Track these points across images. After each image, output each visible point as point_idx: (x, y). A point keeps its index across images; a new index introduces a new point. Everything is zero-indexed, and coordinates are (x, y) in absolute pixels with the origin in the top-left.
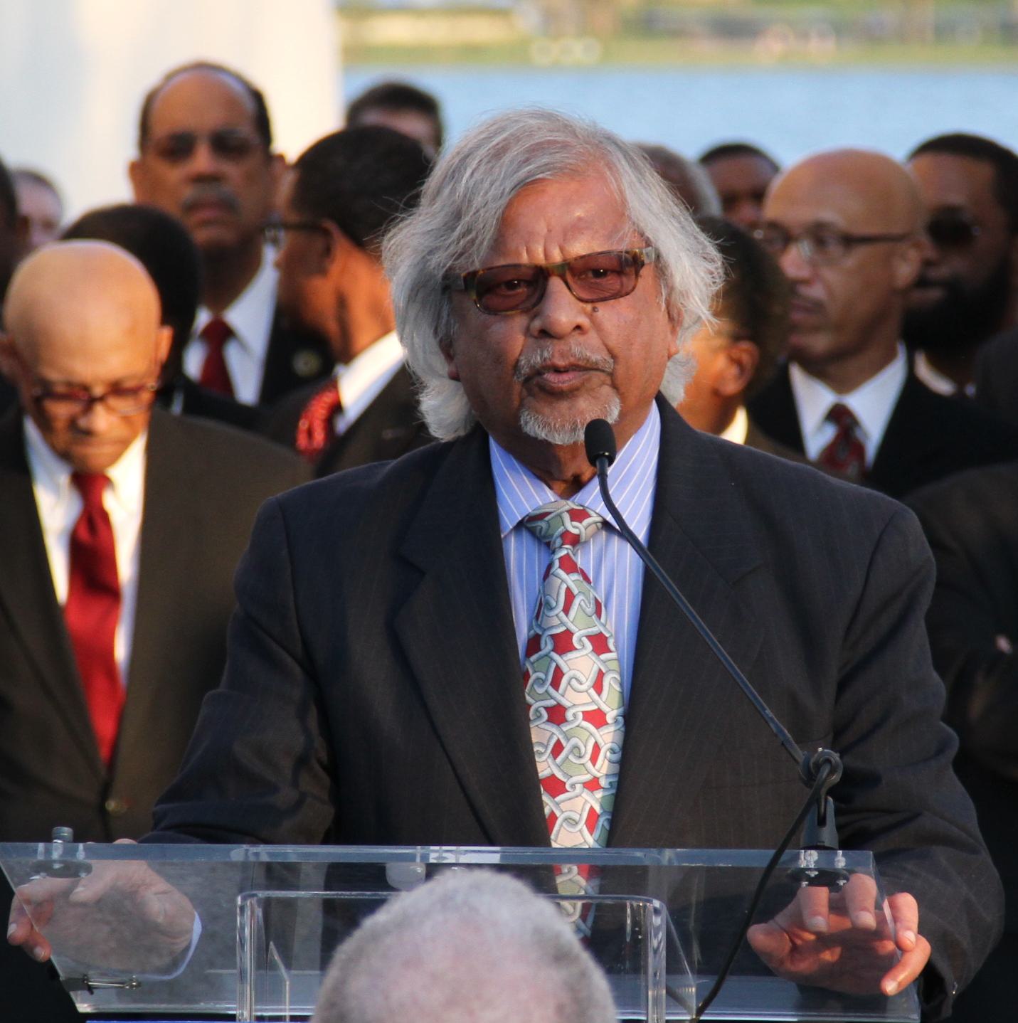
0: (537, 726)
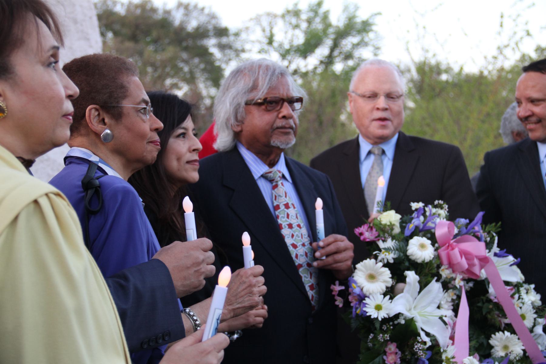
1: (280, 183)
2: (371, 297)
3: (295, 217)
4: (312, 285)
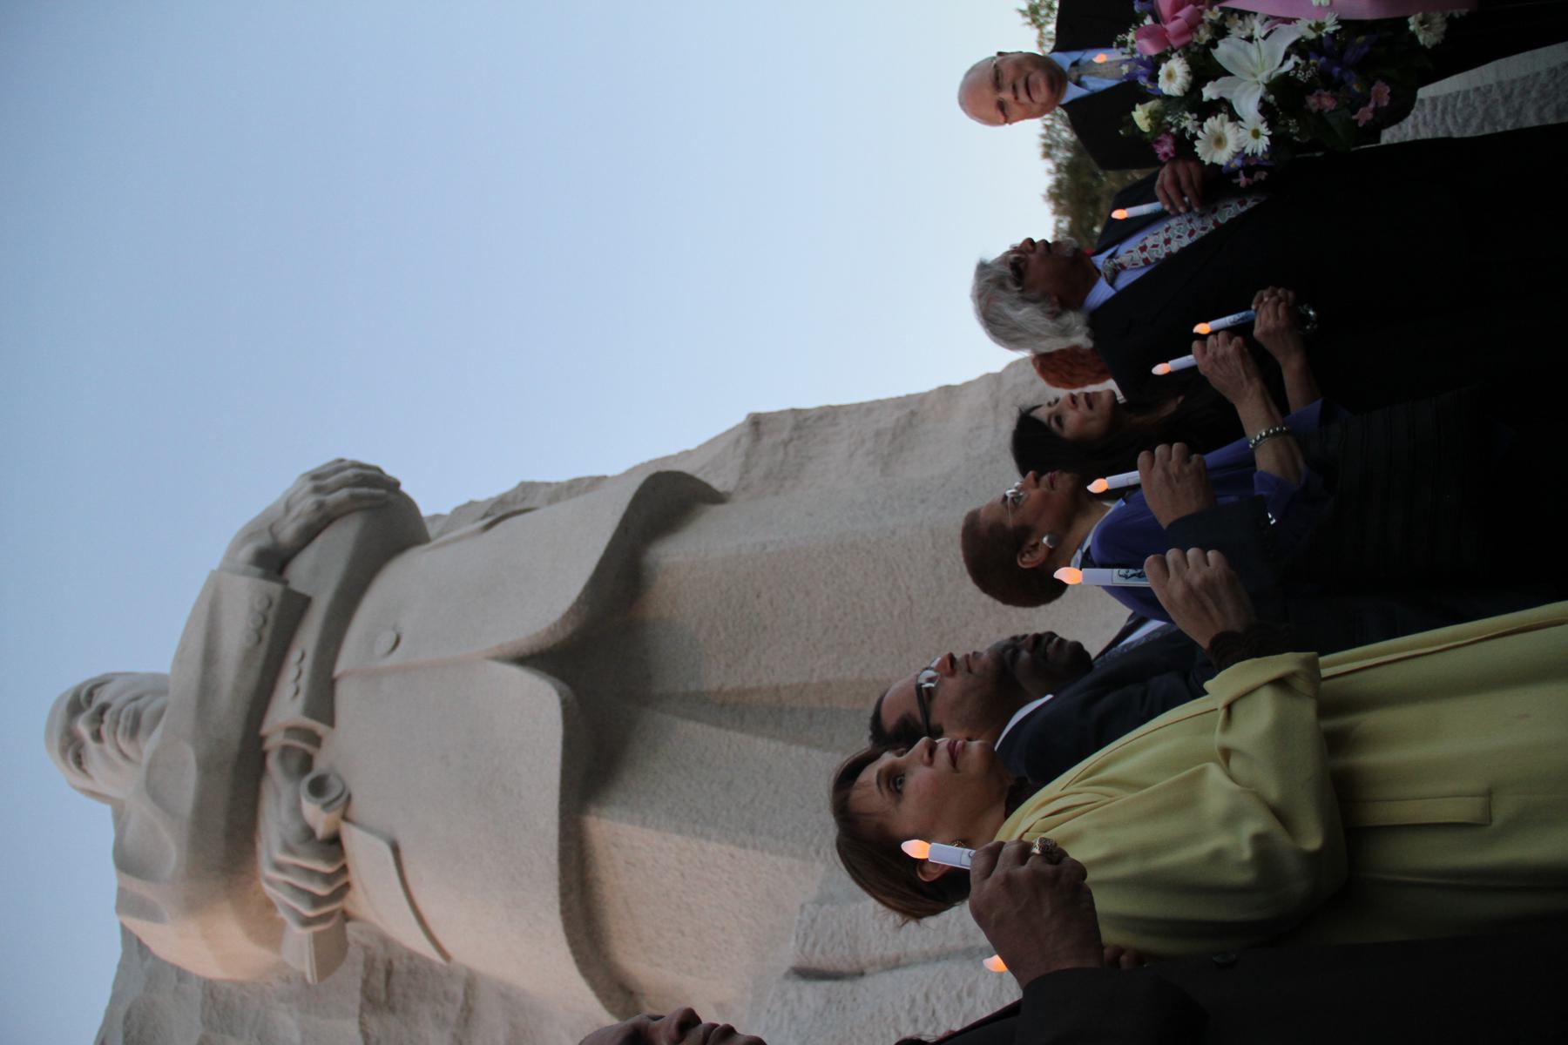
2: (1243, 146)
4: (1239, 203)
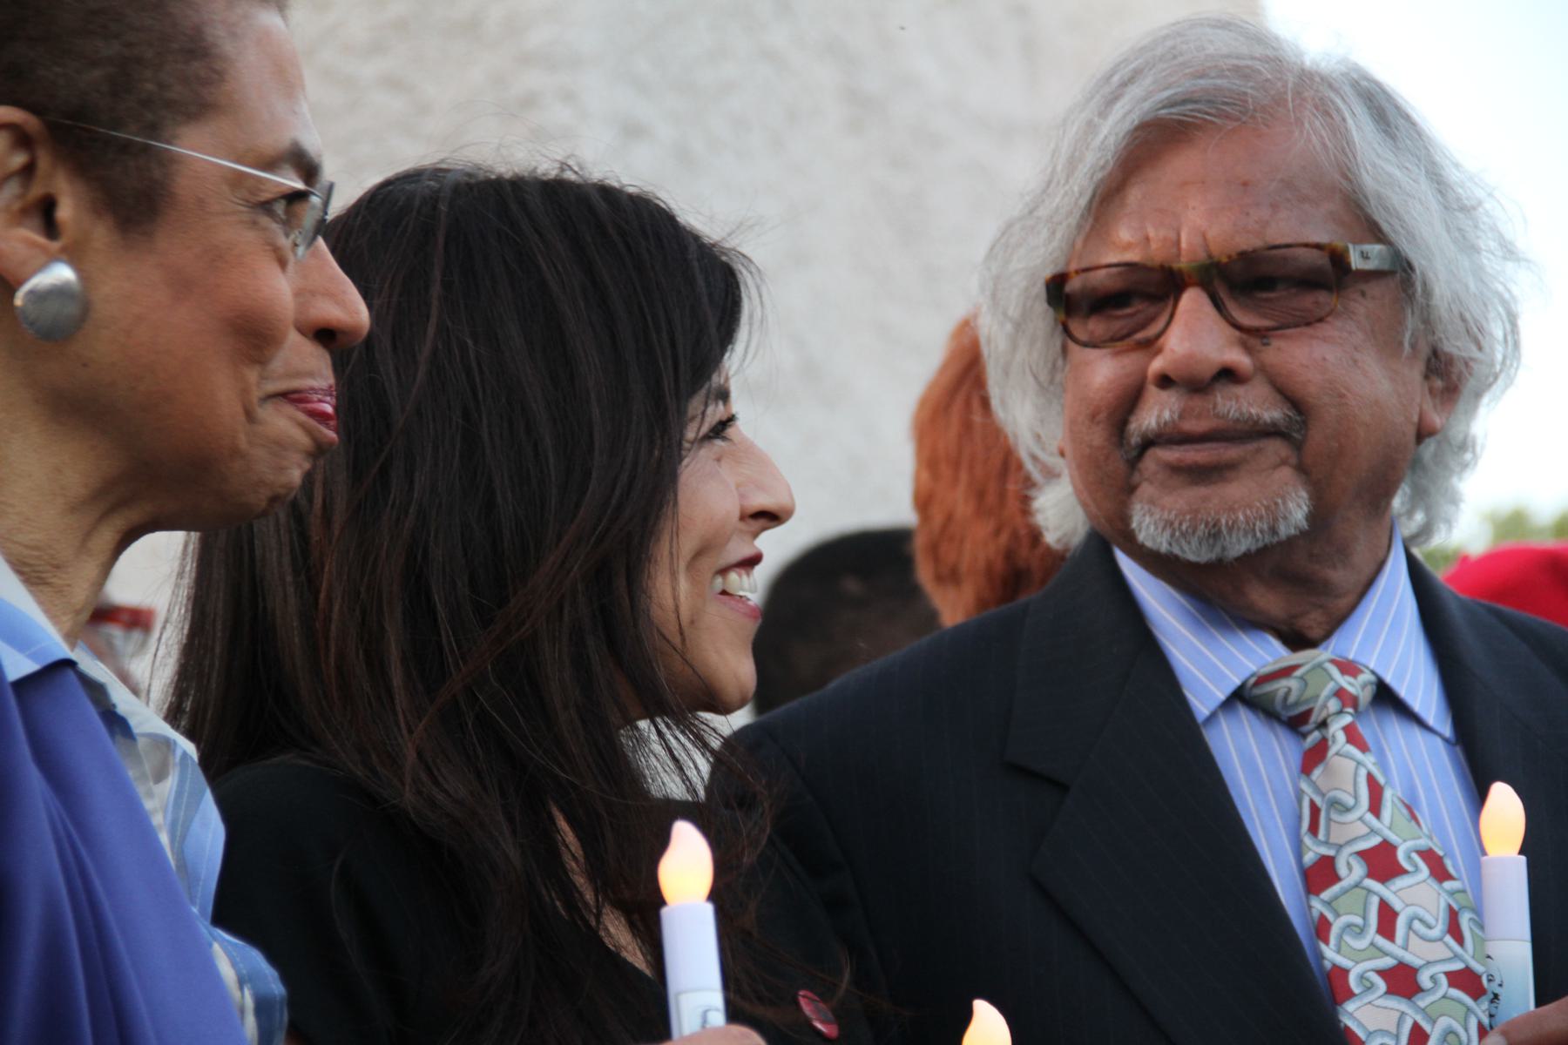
0: (1370, 1003)
1: (1336, 729)
3: (1439, 928)
